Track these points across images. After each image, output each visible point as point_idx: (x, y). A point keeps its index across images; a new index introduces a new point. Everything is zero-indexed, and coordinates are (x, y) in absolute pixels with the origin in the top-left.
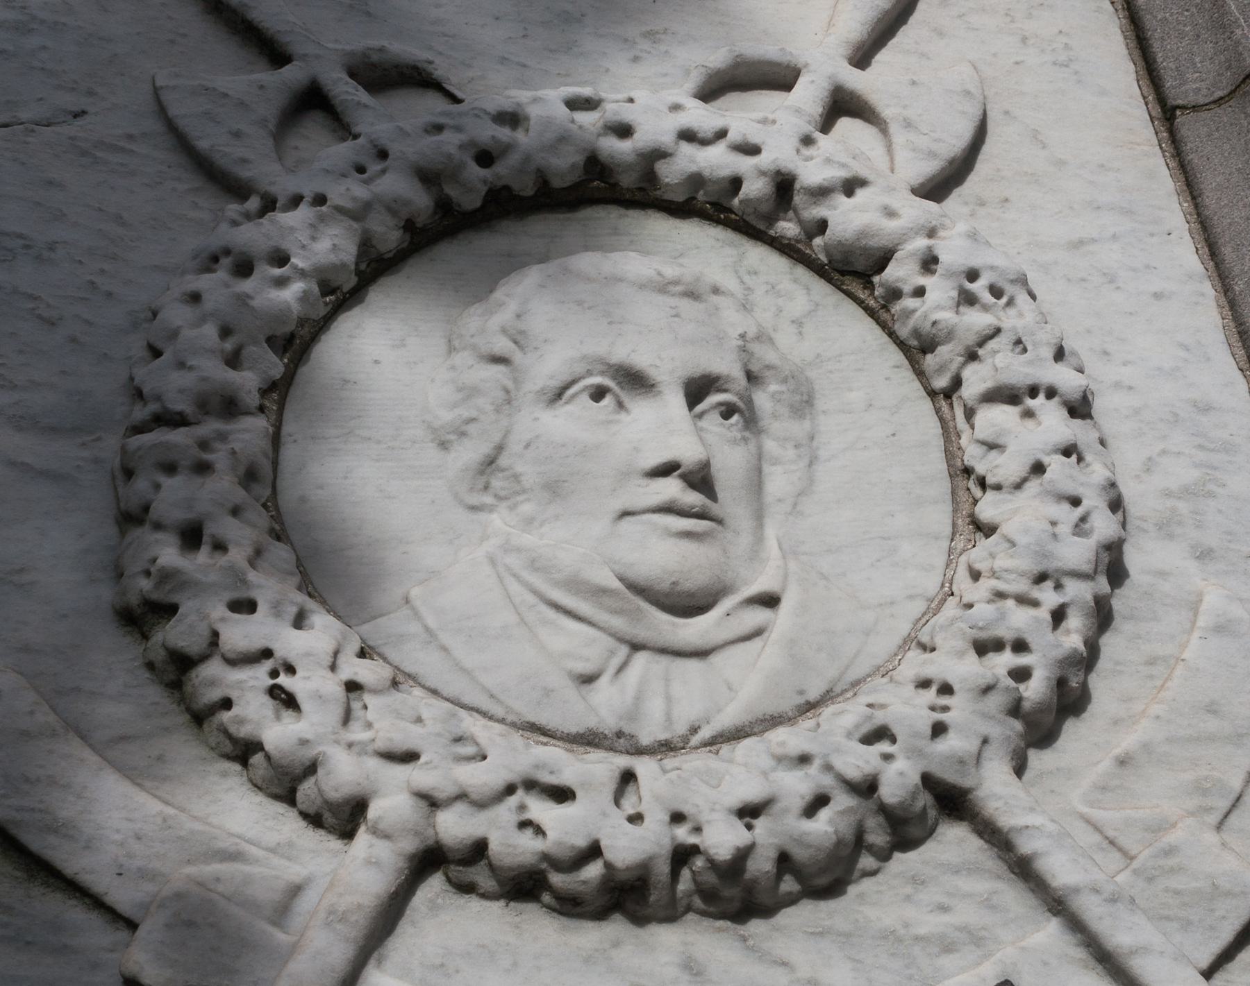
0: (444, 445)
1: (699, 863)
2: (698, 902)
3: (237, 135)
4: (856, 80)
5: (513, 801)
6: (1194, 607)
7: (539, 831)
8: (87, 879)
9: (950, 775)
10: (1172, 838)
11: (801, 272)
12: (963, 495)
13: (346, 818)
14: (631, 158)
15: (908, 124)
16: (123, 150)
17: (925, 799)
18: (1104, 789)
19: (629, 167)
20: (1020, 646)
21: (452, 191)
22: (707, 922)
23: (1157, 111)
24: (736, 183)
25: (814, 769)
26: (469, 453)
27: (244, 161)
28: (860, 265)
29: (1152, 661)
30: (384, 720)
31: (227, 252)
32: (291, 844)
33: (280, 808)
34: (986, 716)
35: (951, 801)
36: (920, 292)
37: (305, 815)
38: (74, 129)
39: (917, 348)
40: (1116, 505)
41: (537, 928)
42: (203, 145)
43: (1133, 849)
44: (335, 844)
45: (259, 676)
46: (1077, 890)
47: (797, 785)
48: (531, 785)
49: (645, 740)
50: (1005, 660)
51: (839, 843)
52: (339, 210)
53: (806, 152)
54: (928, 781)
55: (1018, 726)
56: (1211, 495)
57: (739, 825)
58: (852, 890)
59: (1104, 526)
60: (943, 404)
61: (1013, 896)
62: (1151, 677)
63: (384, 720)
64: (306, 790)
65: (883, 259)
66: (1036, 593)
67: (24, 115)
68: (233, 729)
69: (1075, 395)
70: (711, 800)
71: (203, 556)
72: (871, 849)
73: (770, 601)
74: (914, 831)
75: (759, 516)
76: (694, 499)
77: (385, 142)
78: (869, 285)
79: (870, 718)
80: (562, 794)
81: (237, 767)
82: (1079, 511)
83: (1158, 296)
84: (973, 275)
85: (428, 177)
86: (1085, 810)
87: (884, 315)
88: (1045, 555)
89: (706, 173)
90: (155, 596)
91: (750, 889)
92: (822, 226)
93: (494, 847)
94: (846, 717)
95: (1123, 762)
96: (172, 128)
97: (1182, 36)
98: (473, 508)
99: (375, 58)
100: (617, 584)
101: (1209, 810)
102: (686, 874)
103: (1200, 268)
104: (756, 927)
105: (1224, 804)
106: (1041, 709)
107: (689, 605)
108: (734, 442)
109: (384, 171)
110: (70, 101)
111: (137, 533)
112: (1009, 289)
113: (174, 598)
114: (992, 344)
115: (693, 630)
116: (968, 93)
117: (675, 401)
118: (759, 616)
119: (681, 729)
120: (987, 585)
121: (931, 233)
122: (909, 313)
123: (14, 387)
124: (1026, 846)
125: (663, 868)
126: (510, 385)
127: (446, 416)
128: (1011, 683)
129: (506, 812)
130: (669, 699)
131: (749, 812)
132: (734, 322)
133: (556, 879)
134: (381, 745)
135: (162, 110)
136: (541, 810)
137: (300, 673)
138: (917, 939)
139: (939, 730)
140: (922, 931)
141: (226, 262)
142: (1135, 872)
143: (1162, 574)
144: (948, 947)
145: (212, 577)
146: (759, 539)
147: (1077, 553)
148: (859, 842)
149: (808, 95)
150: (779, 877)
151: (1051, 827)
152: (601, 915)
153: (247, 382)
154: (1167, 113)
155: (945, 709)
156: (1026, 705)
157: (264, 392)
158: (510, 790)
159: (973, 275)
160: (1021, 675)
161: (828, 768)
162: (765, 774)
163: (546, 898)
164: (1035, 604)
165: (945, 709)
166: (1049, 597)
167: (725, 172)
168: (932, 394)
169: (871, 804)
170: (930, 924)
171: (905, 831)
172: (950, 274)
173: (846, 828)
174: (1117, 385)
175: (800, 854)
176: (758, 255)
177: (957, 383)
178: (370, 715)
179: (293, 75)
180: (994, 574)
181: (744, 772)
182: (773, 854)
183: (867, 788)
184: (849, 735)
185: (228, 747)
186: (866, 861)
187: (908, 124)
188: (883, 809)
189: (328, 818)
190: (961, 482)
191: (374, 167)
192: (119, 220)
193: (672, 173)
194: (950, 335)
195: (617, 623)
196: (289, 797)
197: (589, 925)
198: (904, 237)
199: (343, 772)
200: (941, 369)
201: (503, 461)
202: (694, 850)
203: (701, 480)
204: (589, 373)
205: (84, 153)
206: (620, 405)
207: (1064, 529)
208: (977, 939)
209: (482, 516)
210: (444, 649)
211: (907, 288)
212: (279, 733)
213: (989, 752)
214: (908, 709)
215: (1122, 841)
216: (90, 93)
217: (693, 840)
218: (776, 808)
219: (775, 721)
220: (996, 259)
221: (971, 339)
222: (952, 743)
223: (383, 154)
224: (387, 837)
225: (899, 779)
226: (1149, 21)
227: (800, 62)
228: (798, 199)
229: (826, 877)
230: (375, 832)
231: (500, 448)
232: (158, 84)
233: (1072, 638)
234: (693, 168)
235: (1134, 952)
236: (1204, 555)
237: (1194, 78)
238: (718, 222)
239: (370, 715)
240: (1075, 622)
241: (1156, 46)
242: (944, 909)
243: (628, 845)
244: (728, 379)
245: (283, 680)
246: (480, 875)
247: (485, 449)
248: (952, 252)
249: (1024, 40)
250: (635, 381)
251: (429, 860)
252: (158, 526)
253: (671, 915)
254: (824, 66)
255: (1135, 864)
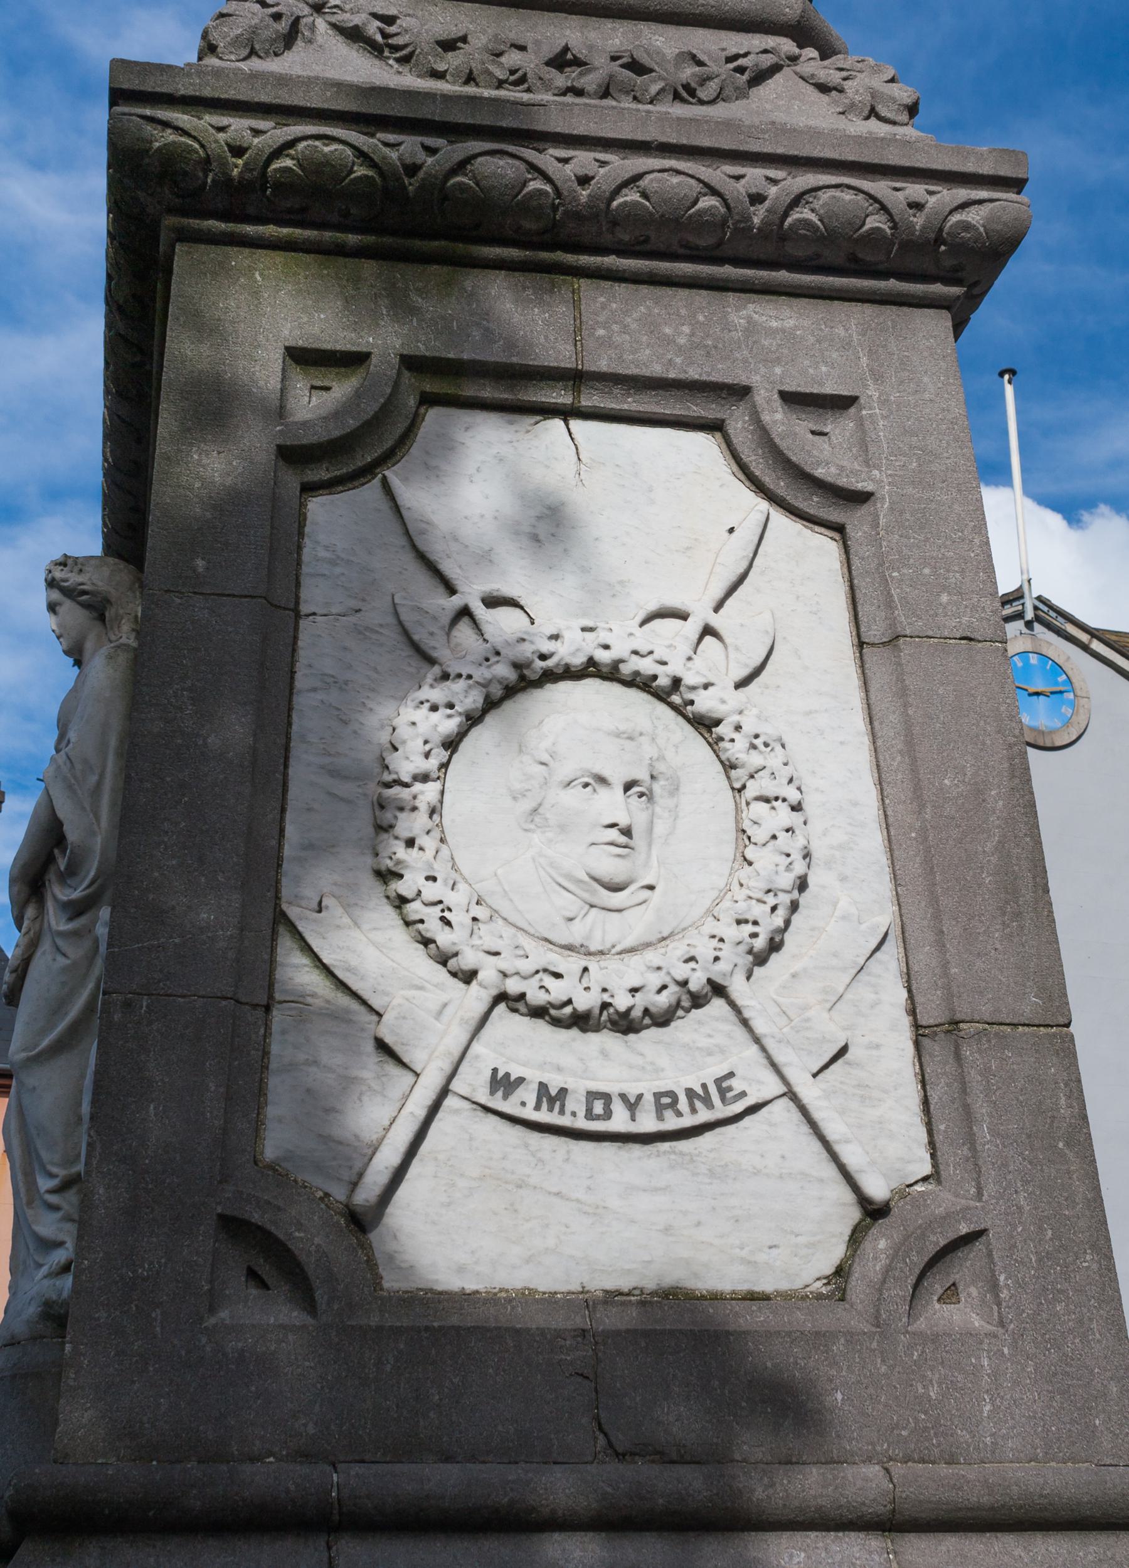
0: (515, 798)
1: (611, 1010)
2: (609, 1025)
3: (432, 634)
4: (716, 621)
5: (538, 976)
6: (835, 904)
7: (547, 991)
8: (361, 992)
9: (719, 980)
10: (810, 1014)
11: (680, 719)
12: (740, 842)
13: (468, 977)
14: (609, 661)
15: (737, 649)
16: (377, 632)
17: (708, 988)
18: (784, 987)
19: (607, 665)
20: (755, 923)
21: (526, 672)
22: (612, 1033)
23: (856, 641)
24: (655, 677)
25: (662, 973)
26: (527, 805)
27: (435, 648)
28: (707, 723)
29: (813, 929)
30: (487, 937)
31: (428, 701)
32: (443, 984)
33: (440, 967)
34: (737, 955)
35: (718, 990)
36: (732, 740)
37: (450, 972)
38: (352, 619)
39: (729, 766)
40: (807, 856)
41: (541, 1027)
42: (416, 637)
43: (792, 1016)
44: (462, 985)
45: (436, 911)
46: (765, 1036)
47: (656, 980)
48: (545, 970)
49: (593, 949)
50: (749, 928)
51: (670, 1006)
52: (477, 683)
53: (689, 664)
54: (709, 981)
55: (750, 958)
56: (851, 849)
57: (629, 995)
58: (673, 1024)
59: (799, 868)
60: (737, 795)
61: (740, 1032)
62: (812, 936)
63: (487, 937)
64: (452, 963)
65: (718, 722)
66: (765, 899)
67: (334, 611)
68: (423, 933)
69: (795, 803)
70: (620, 982)
71: (414, 852)
72: (683, 1008)
73: (651, 888)
74: (701, 1001)
75: (650, 845)
76: (623, 839)
77: (499, 648)
78: (710, 732)
79: (688, 952)
80: (558, 976)
81: (422, 947)
82: (789, 860)
83: (842, 743)
84: (757, 736)
85: (517, 666)
86: (775, 997)
87: (716, 747)
88: (771, 882)
89: (642, 672)
90: (394, 869)
91: (632, 1021)
92: (692, 703)
93: (528, 997)
94: (677, 949)
95: (794, 976)
96: (400, 623)
97: (872, 604)
98: (526, 830)
99: (495, 594)
100: (587, 879)
101: (827, 1001)
102: (605, 1013)
103: (864, 729)
104: (632, 1037)
105: (835, 999)
106: (761, 951)
107: (616, 888)
108: (643, 810)
109: (498, 662)
110: (354, 603)
111: (385, 836)
112: (772, 744)
113: (402, 872)
114: (761, 773)
115: (616, 900)
116: (767, 632)
117: (620, 790)
118: (647, 893)
119: (608, 945)
120: (745, 892)
121: (741, 713)
122: (726, 750)
123: (330, 755)
124: (747, 1014)
125: (597, 1011)
126: (547, 776)
127: (517, 786)
128: (749, 940)
129: (534, 982)
130: (604, 931)
131: (634, 991)
132: (649, 750)
133: (553, 1012)
134: (486, 948)
135: (396, 614)
136: (549, 981)
137: (454, 912)
138: (698, 1048)
139: (717, 959)
140: (699, 1045)
141: (427, 705)
142: (792, 1028)
143: (824, 887)
144: (710, 1054)
145: (419, 865)
146: (649, 856)
147: (786, 880)
148: (678, 1005)
149: (692, 628)
150: (643, 1018)
151: (758, 1007)
152: (568, 1027)
153: (432, 764)
154: (861, 644)
155: (720, 949)
156: (755, 950)
157: (439, 770)
158: (537, 972)
159: (757, 736)
160: (754, 935)
161: (669, 973)
162: (642, 974)
163: (547, 1018)
164: (765, 903)
165: (720, 949)
166: (771, 900)
167: (651, 672)
168: (733, 789)
169: (685, 990)
170: (704, 1042)
171: (698, 1001)
172: (747, 736)
173: (673, 1000)
174: (817, 790)
175: (653, 1009)
176: (662, 709)
177: (744, 787)
178: (482, 933)
179: (456, 601)
180: (748, 888)
181: (633, 971)
182: (642, 1009)
183: (684, 984)
184: (679, 959)
185: (420, 938)
186: (680, 1013)
187: (737, 649)
188: (689, 992)
189: (460, 974)
190: (740, 835)
191: (494, 659)
192: (375, 670)
193: (625, 670)
194: (743, 766)
195: (586, 896)
196: (444, 963)
197: (564, 1030)
198: (728, 715)
199: (468, 959)
200: (738, 779)
201: (540, 811)
202: (610, 1004)
203: (627, 832)
204: (583, 776)
205: (360, 633)
206: (595, 790)
207: (782, 868)
208: (722, 1051)
209: (529, 834)
210: (511, 900)
211: (727, 738)
212: (444, 938)
213: (737, 969)
214: (705, 949)
215: (788, 1013)
216: (364, 600)
217: (610, 1000)
218: (644, 990)
219: (648, 945)
220: (768, 730)
221: (752, 770)
222: (721, 966)
223: (498, 653)
224: (485, 988)
225: (697, 982)
226: (859, 595)
227: (690, 610)
228: (682, 689)
229: (662, 1019)
230: (480, 985)
231: (540, 805)
232: (396, 601)
233: (778, 921)
234: (637, 668)
235: (785, 1065)
236: (843, 879)
237: (875, 632)
238: (645, 691)
239: (482, 933)
240: (781, 913)
241: (859, 608)
242: (710, 1036)
243: (584, 1001)
244: (643, 781)
245: (446, 914)
246: (521, 1006)
247: (534, 805)
248: (748, 728)
249: (798, 597)
250: (602, 780)
251: (502, 997)
252: (397, 838)
253: (597, 1029)
254: (702, 613)
255: (793, 1024)
